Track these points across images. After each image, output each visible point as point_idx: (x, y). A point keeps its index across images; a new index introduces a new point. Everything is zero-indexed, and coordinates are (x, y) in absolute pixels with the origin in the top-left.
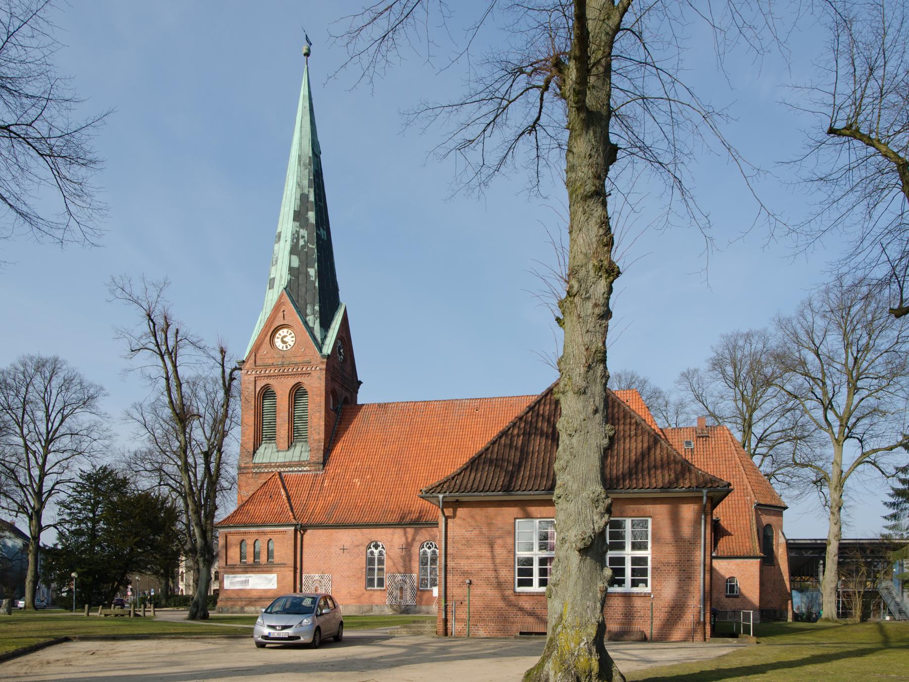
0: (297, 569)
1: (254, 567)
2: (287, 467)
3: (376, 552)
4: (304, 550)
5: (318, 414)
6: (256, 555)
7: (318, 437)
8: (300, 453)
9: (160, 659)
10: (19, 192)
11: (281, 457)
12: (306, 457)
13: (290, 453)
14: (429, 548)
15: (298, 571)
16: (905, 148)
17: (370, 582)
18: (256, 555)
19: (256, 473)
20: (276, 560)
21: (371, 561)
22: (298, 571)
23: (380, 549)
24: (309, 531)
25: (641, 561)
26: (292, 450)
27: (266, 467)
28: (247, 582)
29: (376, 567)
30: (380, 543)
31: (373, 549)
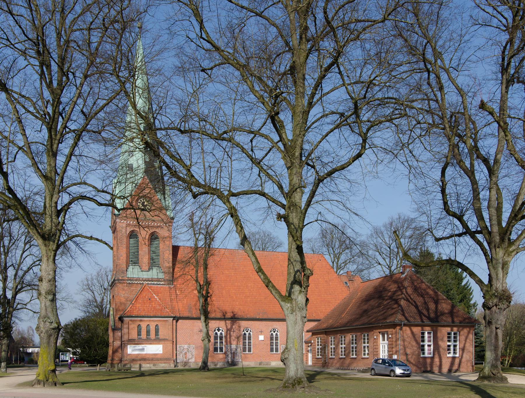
0: (175, 343)
1: (149, 341)
2: (150, 281)
3: (274, 334)
4: (178, 331)
5: (168, 252)
6: (148, 332)
7: (168, 265)
8: (154, 273)
9: (248, 379)
10: (355, 237)
11: (145, 275)
12: (161, 276)
13: (150, 273)
14: (247, 331)
15: (175, 343)
16: (299, 1)
17: (272, 350)
18: (148, 332)
19: (129, 283)
20: (161, 335)
21: (272, 339)
22: (175, 343)
23: (221, 331)
24: (180, 321)
25: (449, 341)
26: (151, 271)
27: (136, 280)
28: (143, 349)
29: (247, 341)
30: (220, 328)
31: (217, 331)
